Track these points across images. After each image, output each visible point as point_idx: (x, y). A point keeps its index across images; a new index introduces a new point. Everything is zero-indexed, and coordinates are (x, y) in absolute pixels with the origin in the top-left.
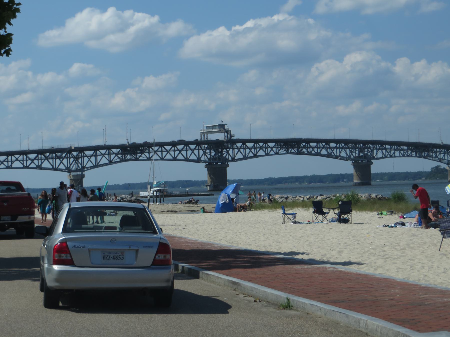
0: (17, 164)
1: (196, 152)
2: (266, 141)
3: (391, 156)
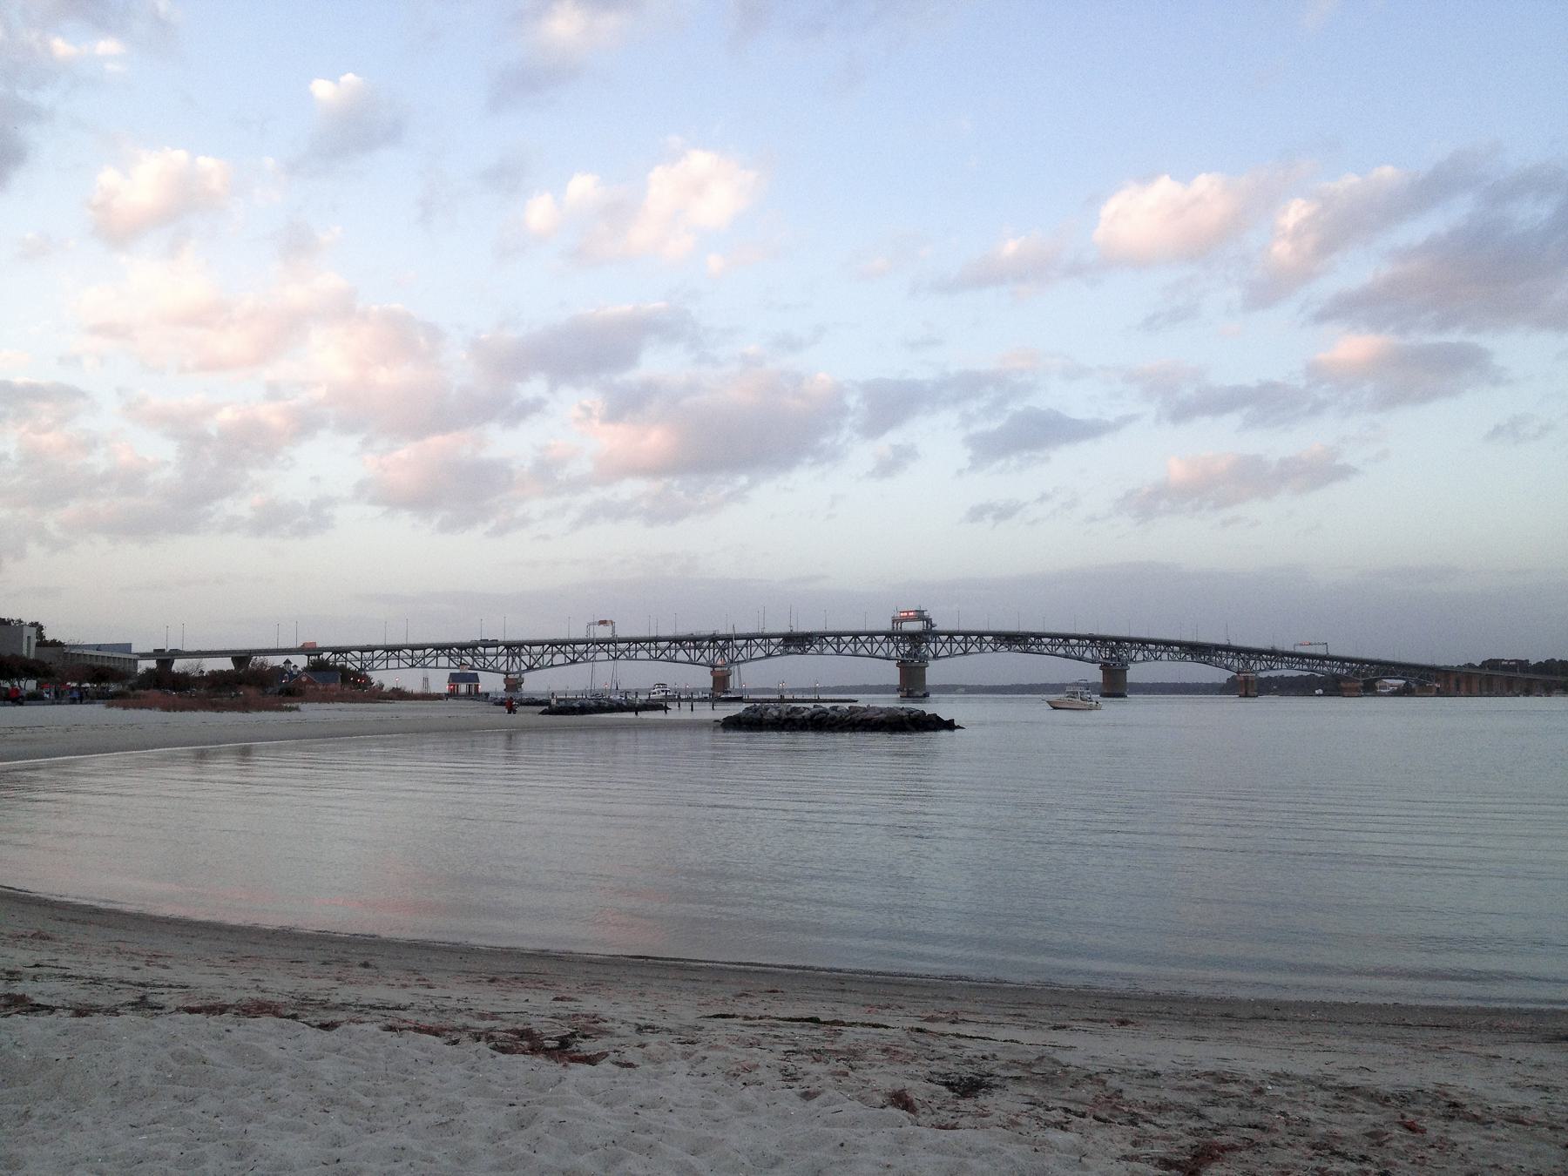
0: (643, 654)
1: (885, 646)
2: (981, 635)
3: (1156, 659)
